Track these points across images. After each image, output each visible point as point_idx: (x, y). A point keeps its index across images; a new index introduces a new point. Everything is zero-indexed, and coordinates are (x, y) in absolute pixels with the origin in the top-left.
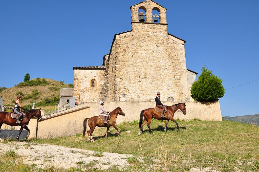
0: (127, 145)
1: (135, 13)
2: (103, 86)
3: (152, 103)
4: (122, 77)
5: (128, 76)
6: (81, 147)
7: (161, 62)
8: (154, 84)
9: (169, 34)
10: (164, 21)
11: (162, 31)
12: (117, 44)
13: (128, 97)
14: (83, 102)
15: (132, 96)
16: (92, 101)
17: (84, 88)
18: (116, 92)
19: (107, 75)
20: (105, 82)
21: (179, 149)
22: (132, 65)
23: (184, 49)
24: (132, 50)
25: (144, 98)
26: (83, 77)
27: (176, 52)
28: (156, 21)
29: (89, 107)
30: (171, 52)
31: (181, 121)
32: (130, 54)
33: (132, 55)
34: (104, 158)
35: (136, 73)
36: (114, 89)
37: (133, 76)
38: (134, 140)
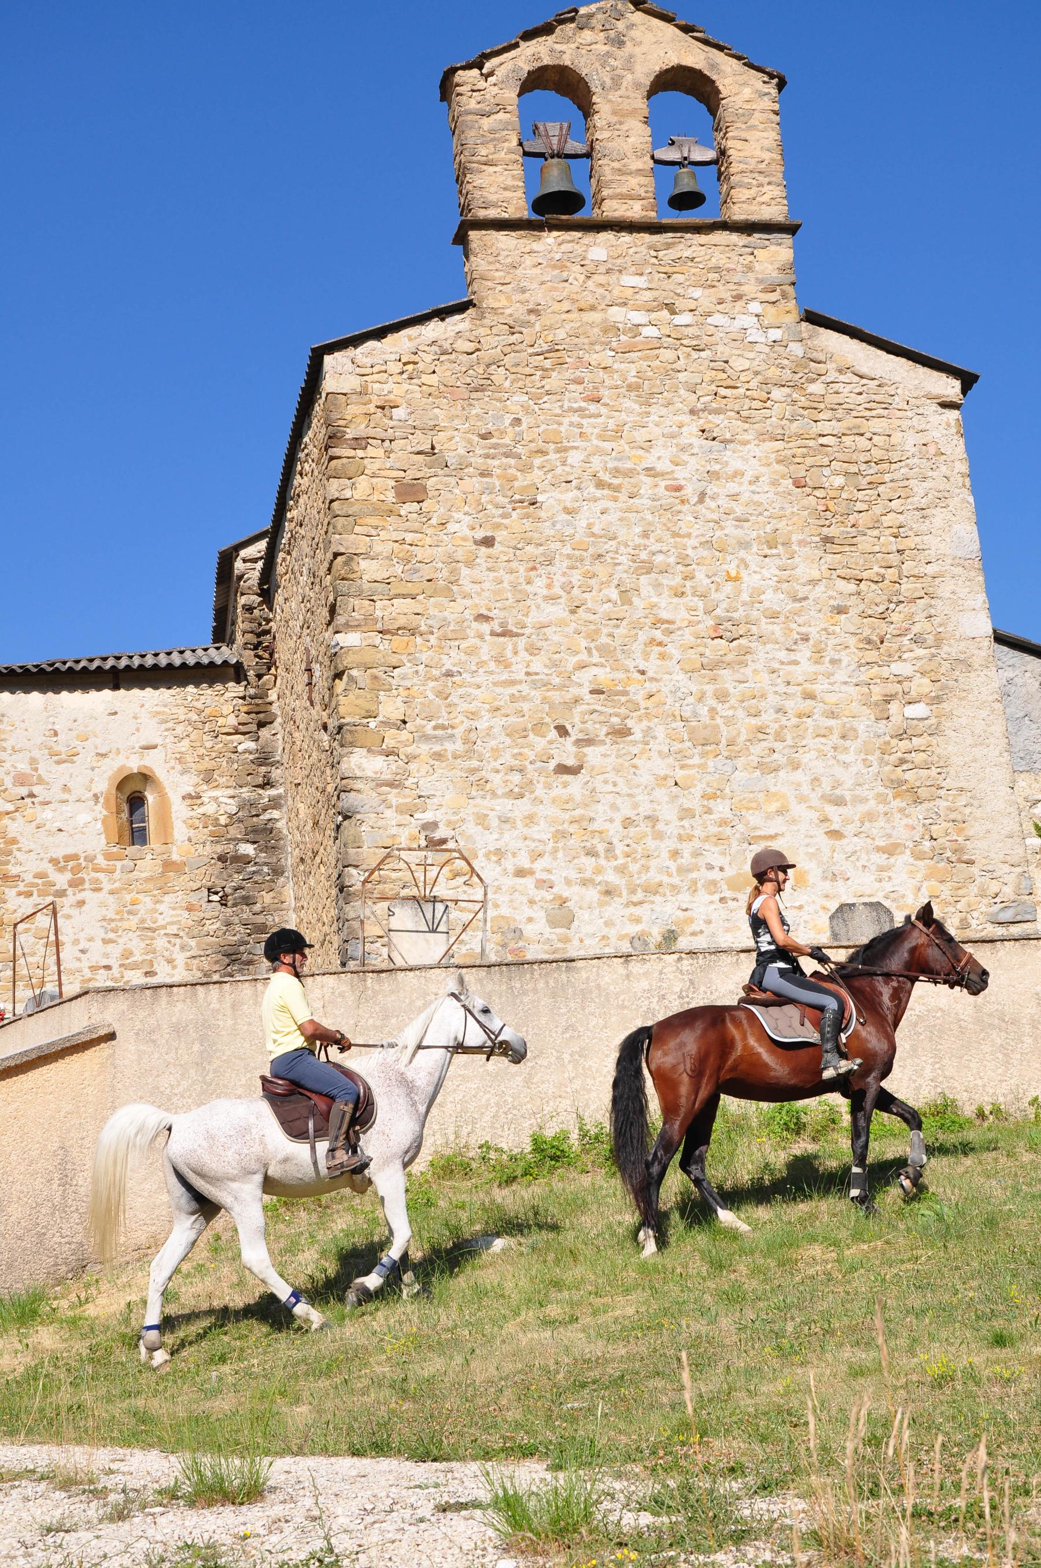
0: (482, 1371)
1: (493, 137)
2: (234, 832)
3: (686, 963)
4: (404, 735)
5: (459, 732)
6: (49, 1427)
7: (750, 580)
8: (698, 790)
9: (812, 318)
10: (771, 207)
11: (750, 289)
12: (334, 438)
13: (467, 917)
14: (51, 988)
15: (502, 907)
16: (136, 978)
17: (54, 861)
18: (355, 877)
19: (261, 725)
20: (246, 793)
21: (977, 1384)
22: (485, 628)
23: (957, 448)
24: (474, 483)
25: (609, 924)
26: (33, 761)
27: (887, 477)
28: (688, 205)
29: (111, 1036)
30: (839, 481)
31: (969, 1121)
32: (462, 526)
33: (480, 534)
34: (278, 1511)
35: (524, 698)
36: (330, 852)
37: (499, 722)
38: (548, 1323)
